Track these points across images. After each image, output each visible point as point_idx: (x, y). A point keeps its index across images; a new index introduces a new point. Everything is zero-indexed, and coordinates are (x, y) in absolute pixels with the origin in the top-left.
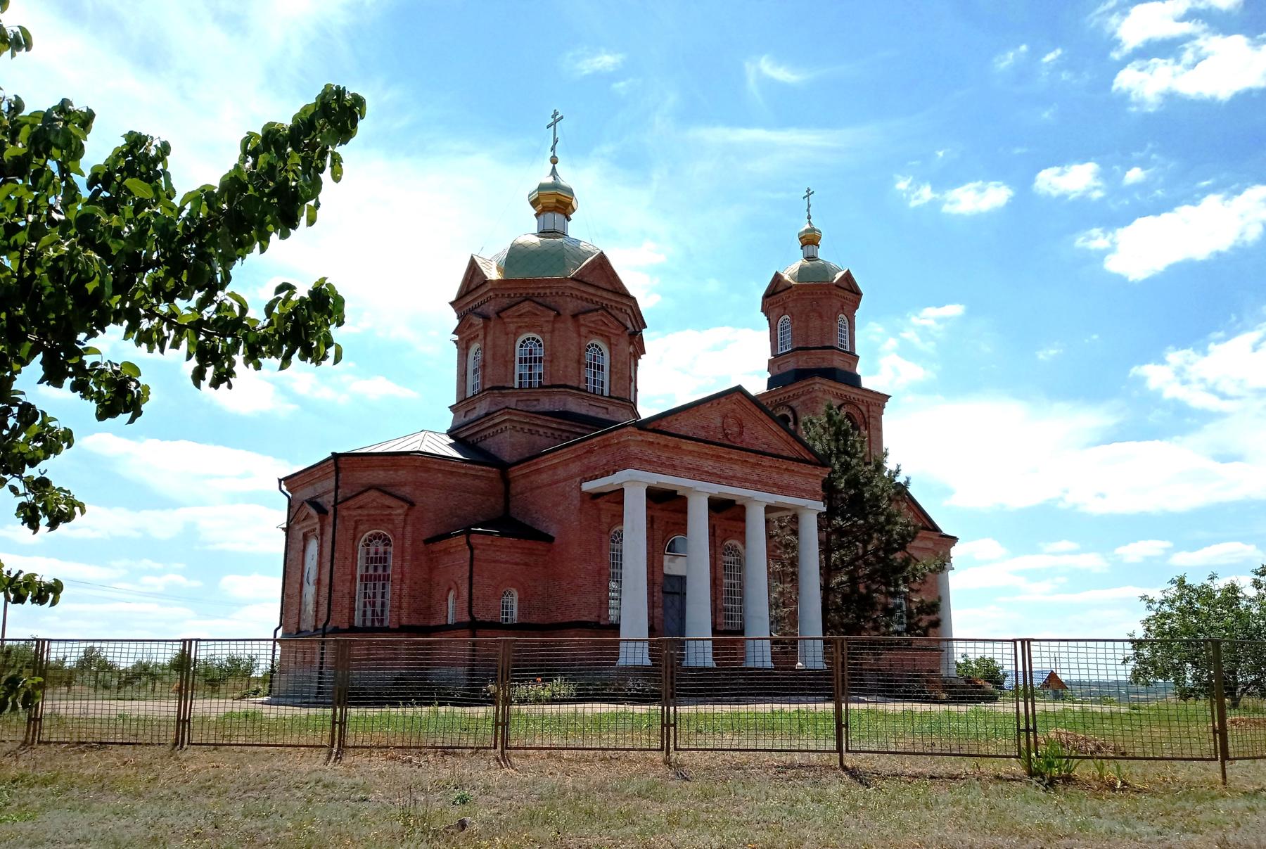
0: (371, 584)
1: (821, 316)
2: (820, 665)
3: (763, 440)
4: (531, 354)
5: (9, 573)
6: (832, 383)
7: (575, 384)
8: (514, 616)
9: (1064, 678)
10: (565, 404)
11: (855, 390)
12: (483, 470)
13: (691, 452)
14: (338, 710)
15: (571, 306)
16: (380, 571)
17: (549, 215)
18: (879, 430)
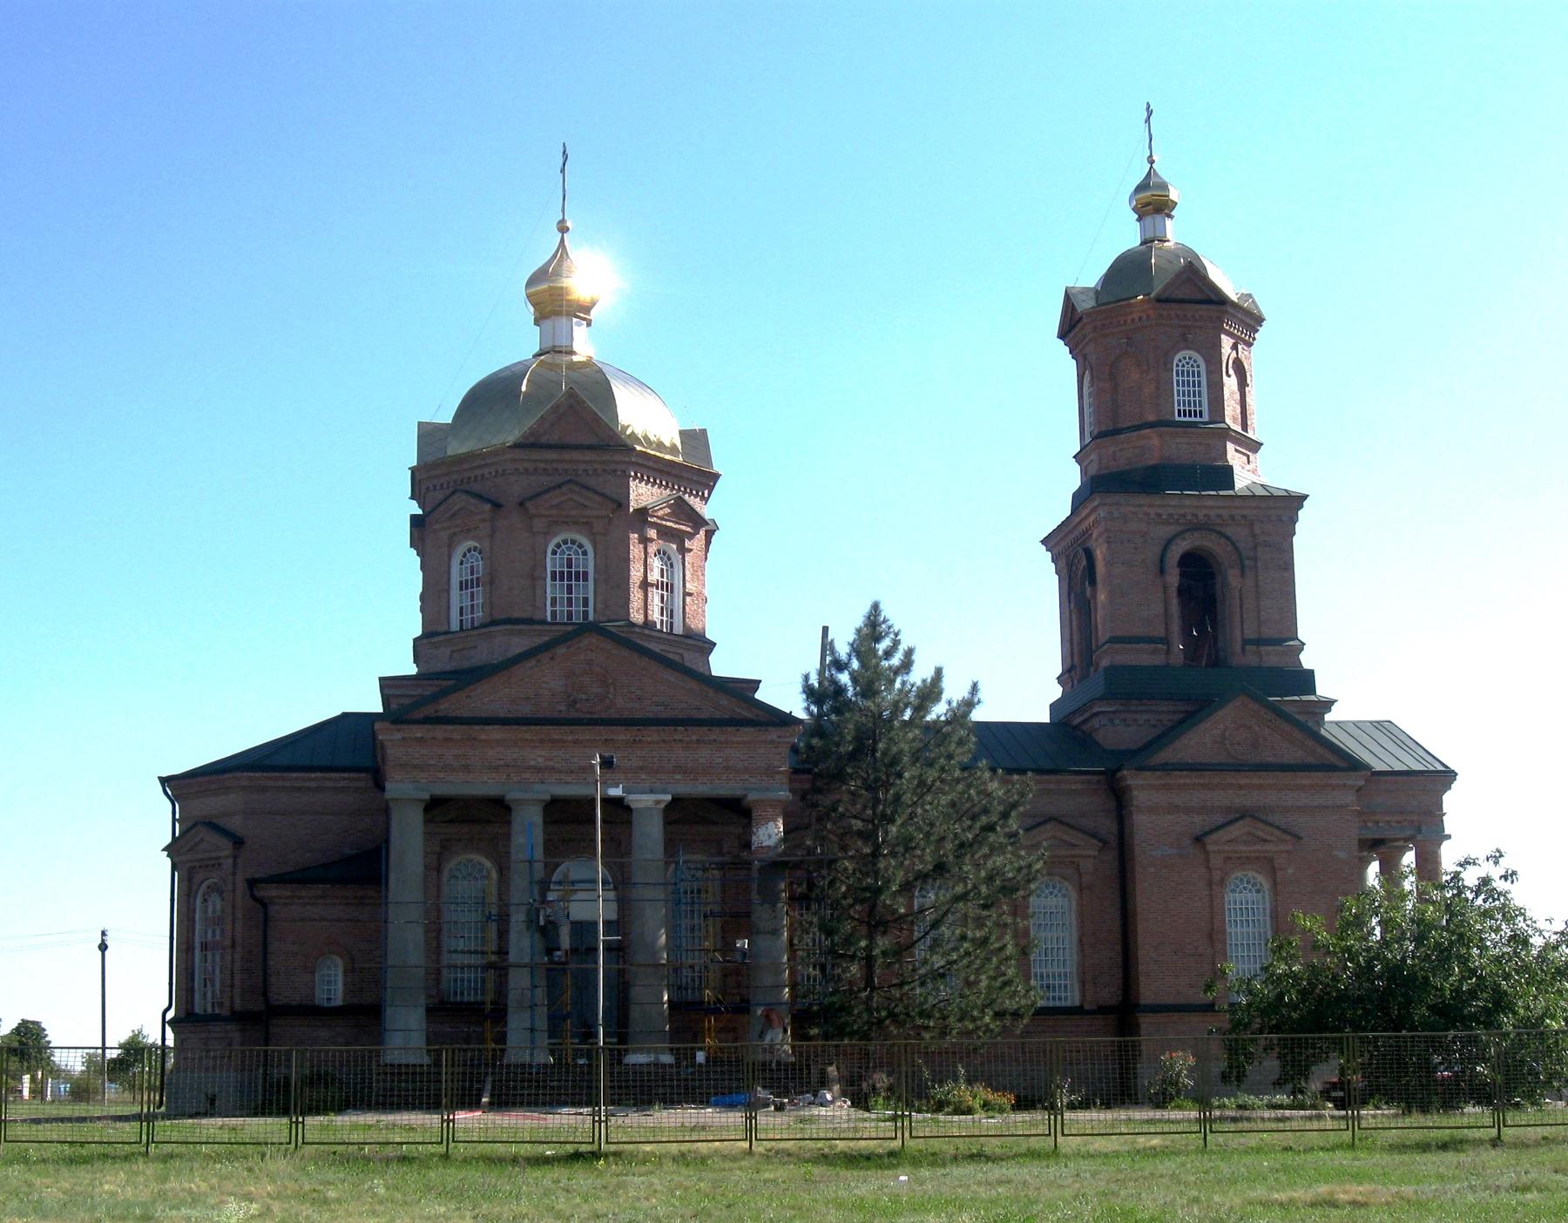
3: (655, 699)
4: (570, 566)
5: (931, 692)
12: (345, 779)
18: (1287, 566)
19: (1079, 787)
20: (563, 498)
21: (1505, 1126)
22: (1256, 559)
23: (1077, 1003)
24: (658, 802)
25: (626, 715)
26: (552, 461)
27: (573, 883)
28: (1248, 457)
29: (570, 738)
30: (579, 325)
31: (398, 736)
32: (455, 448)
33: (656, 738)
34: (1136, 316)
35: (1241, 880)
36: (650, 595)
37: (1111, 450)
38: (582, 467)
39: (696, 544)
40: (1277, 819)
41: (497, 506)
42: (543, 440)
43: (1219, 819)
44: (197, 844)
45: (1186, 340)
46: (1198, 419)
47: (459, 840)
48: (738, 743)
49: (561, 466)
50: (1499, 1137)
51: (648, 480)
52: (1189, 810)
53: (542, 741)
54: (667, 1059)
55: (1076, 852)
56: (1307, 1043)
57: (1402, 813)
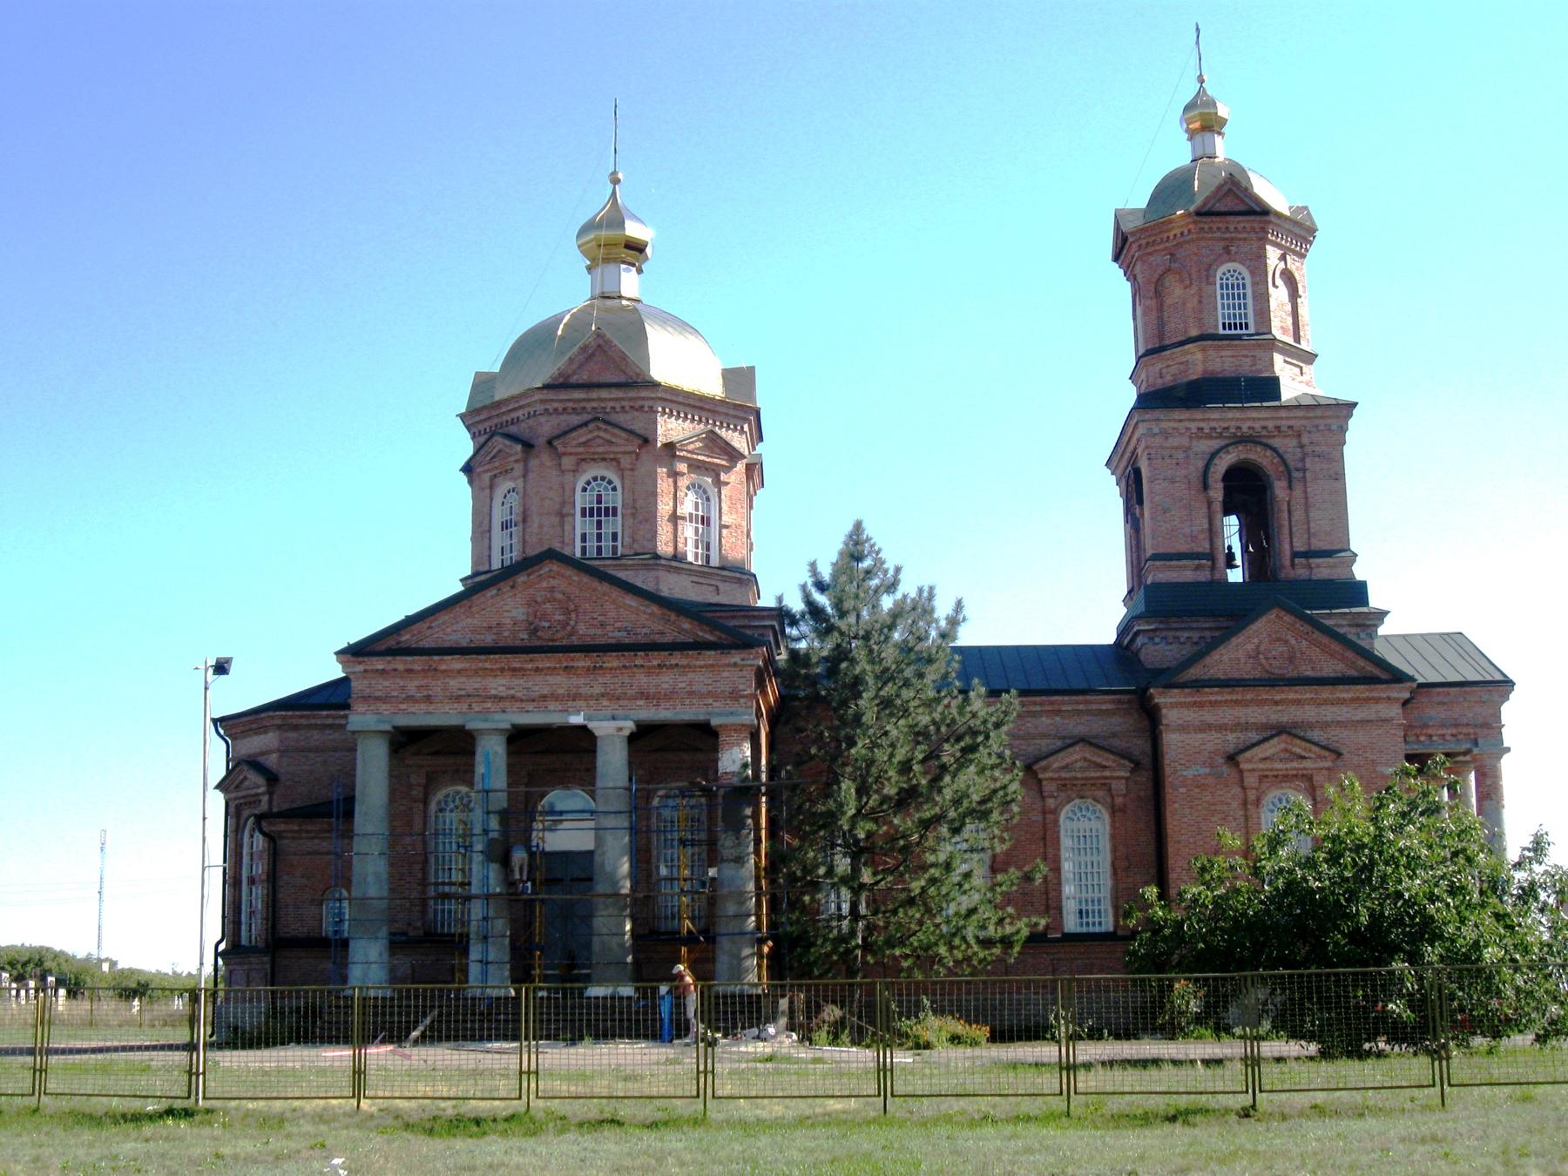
4: (599, 502)
13: (459, 672)
18: (1339, 476)
19: (1110, 707)
20: (590, 436)
21: (1261, 1091)
22: (1304, 470)
23: (1111, 929)
24: (620, 729)
25: (589, 641)
26: (579, 401)
27: (561, 813)
28: (1301, 368)
29: (530, 666)
30: (628, 271)
31: (361, 668)
32: (501, 394)
33: (615, 664)
34: (1177, 231)
35: (1280, 801)
36: (680, 528)
37: (1157, 369)
38: (611, 404)
39: (735, 476)
40: (1315, 735)
41: (528, 446)
42: (573, 380)
43: (1254, 736)
44: (242, 782)
45: (1228, 252)
46: (1244, 331)
47: (445, 772)
48: (701, 667)
49: (589, 406)
50: (1253, 1107)
51: (686, 417)
52: (1222, 728)
53: (502, 670)
54: (627, 991)
55: (1107, 773)
56: (1098, 986)
57: (1456, 725)
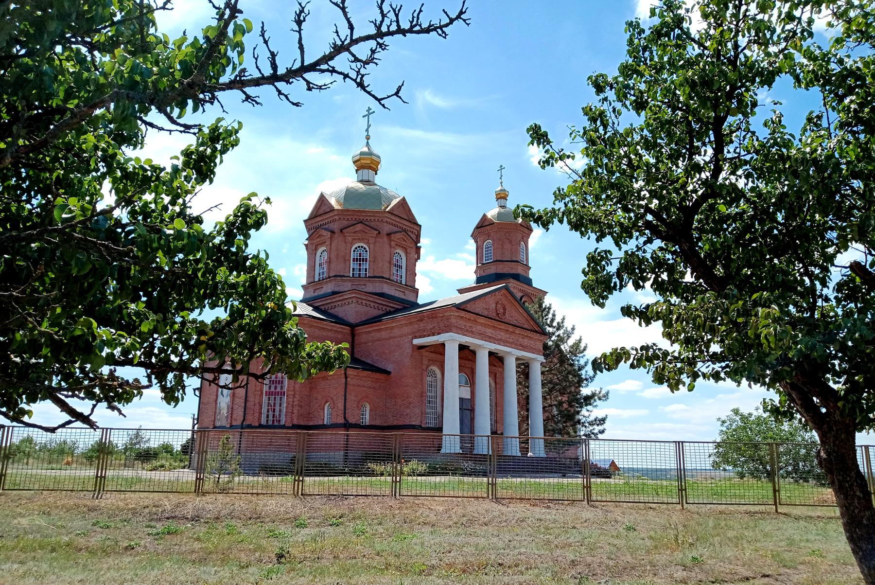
0: (272, 398)
1: (511, 242)
2: (543, 454)
4: (360, 256)
6: (518, 283)
7: (388, 277)
8: (367, 420)
9: (620, 465)
10: (382, 288)
11: (530, 288)
14: (490, 479)
15: (387, 228)
16: (279, 389)
17: (366, 171)
